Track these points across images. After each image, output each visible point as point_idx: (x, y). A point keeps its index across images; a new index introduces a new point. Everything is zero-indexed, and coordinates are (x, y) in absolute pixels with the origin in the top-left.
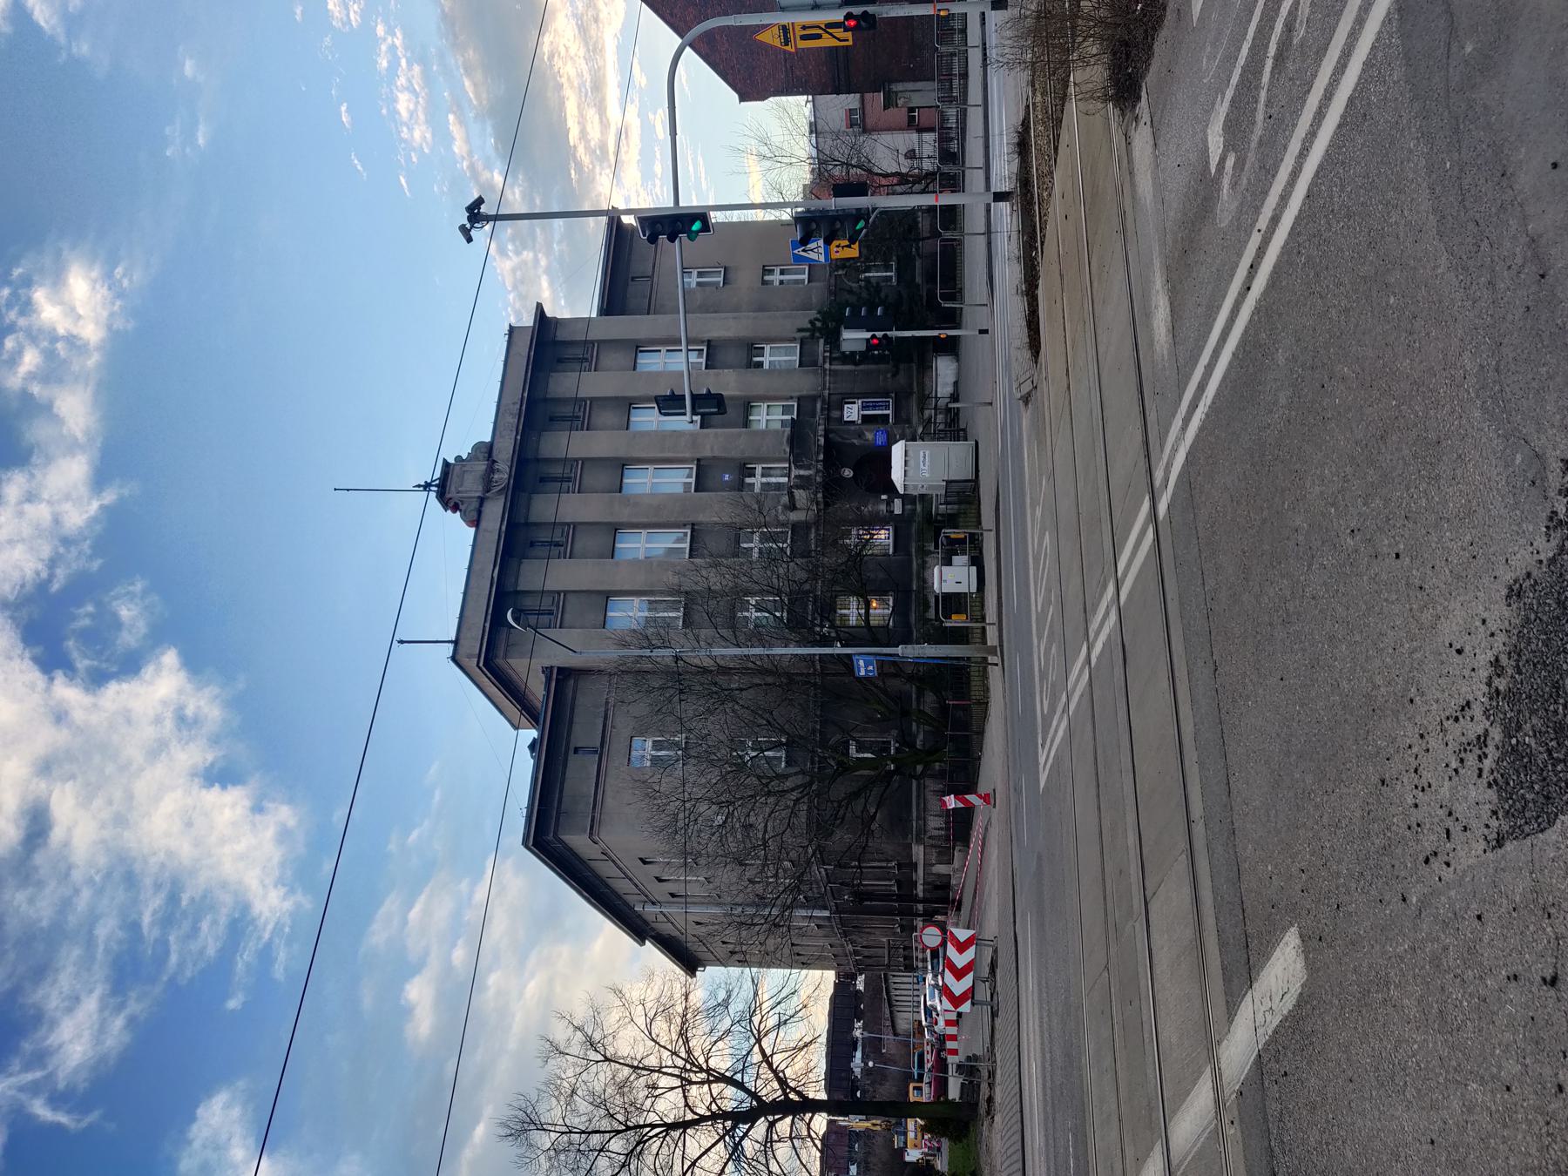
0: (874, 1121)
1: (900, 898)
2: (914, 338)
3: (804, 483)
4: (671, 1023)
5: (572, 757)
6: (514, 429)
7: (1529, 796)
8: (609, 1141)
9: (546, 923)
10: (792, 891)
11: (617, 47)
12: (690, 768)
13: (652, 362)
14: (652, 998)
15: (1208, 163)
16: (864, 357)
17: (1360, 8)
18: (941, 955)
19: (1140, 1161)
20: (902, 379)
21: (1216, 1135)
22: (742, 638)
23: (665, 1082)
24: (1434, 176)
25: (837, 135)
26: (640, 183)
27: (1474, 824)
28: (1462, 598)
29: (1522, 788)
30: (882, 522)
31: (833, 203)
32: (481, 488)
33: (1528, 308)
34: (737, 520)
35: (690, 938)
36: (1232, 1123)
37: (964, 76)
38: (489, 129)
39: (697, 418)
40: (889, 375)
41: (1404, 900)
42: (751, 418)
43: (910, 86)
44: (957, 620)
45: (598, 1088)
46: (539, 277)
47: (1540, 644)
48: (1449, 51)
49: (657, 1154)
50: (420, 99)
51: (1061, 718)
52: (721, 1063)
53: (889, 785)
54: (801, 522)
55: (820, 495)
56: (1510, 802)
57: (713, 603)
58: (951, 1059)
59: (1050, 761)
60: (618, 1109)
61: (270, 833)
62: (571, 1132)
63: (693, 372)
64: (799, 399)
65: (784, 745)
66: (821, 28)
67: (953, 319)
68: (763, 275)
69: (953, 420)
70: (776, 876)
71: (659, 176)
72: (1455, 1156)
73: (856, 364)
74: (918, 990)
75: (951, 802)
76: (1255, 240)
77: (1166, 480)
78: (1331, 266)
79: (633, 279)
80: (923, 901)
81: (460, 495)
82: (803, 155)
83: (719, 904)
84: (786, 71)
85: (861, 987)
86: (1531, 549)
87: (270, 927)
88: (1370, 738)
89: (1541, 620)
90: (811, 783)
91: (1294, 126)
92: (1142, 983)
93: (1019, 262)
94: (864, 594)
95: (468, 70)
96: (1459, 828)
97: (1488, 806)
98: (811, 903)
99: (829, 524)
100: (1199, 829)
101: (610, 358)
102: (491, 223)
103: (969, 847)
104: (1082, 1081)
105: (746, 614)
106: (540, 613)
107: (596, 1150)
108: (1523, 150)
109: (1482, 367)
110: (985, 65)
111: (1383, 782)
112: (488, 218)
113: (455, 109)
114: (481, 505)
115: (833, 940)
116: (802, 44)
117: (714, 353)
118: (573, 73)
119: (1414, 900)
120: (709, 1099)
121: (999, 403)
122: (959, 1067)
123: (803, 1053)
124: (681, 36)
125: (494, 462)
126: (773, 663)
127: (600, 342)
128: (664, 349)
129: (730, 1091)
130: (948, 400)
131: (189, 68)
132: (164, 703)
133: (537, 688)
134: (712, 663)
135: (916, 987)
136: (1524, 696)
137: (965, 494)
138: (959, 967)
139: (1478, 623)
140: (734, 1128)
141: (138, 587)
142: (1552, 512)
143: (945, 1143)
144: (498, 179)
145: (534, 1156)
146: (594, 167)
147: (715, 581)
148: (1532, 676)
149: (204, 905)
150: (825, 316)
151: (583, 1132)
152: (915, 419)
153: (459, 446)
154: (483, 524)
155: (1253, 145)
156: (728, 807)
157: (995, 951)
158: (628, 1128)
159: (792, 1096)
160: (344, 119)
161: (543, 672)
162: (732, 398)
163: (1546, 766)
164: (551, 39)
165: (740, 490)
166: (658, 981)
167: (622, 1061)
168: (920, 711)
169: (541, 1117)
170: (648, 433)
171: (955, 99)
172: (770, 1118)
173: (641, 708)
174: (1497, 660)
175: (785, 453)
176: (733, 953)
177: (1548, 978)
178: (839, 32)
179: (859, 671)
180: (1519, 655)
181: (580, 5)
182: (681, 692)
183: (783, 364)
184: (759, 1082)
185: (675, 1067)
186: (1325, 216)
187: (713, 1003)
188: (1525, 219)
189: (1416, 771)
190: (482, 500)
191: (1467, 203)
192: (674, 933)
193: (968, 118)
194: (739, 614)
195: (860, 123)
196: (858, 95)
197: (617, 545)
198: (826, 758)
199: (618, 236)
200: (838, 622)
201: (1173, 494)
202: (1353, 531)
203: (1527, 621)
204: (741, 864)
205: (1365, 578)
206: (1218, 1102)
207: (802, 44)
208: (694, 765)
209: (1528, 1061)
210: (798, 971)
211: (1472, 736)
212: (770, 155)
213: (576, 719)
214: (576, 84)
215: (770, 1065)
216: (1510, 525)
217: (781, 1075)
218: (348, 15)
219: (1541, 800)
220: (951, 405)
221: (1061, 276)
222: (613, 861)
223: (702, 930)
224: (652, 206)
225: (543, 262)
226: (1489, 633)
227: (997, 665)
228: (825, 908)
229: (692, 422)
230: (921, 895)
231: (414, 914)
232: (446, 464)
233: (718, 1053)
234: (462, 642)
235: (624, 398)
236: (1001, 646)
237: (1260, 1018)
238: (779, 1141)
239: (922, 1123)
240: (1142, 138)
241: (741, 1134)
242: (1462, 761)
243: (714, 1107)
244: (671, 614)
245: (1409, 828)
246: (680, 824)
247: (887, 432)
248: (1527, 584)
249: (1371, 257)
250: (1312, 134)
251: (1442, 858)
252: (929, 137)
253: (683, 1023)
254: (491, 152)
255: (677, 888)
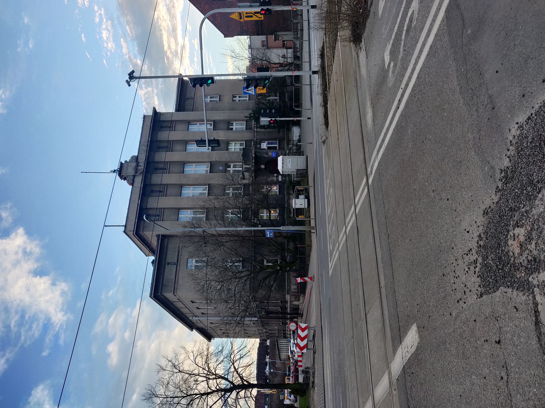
0: (273, 390)
1: (281, 313)
2: (285, 120)
3: (248, 170)
4: (202, 358)
5: (167, 266)
6: (146, 151)
7: (491, 281)
8: (181, 400)
9: (159, 323)
10: (244, 311)
11: (181, 16)
12: (208, 269)
13: (194, 128)
14: (196, 350)
15: (384, 65)
16: (268, 127)
17: (434, 16)
18: (296, 333)
19: (364, 403)
20: (281, 134)
21: (390, 393)
22: (226, 224)
23: (200, 379)
24: (458, 73)
25: (258, 49)
26: (189, 64)
27: (473, 289)
28: (469, 214)
29: (488, 278)
30: (275, 183)
31: (258, 74)
32: (134, 172)
33: (489, 119)
34: (225, 183)
35: (209, 328)
36: (395, 389)
37: (302, 30)
38: (136, 44)
39: (210, 148)
40: (277, 133)
41: (451, 315)
42: (229, 147)
43: (283, 33)
44: (301, 218)
45: (177, 382)
46: (154, 97)
47: (494, 230)
48: (463, 32)
49: (198, 404)
50: (111, 33)
51: (336, 252)
52: (220, 372)
53: (278, 274)
54: (247, 184)
55: (253, 174)
56: (485, 282)
57: (216, 212)
58: (300, 369)
59: (333, 266)
60: (184, 389)
61: (58, 293)
62: (167, 397)
63: (209, 132)
64: (246, 141)
65: (241, 261)
66: (252, 14)
67: (298, 114)
68: (233, 98)
69: (299, 149)
70: (239, 306)
71: (196, 62)
72: (468, 400)
73: (265, 129)
74: (288, 345)
75: (299, 280)
76: (400, 91)
77: (372, 171)
78: (425, 101)
79: (187, 99)
80: (289, 314)
81: (127, 174)
82: (247, 56)
83: (219, 316)
84: (240, 27)
85: (268, 344)
86: (490, 198)
87: (58, 326)
88: (439, 260)
89: (494, 222)
90: (251, 274)
91: (413, 54)
92: (365, 342)
93: (321, 95)
94: (269, 209)
95: (128, 23)
96: (468, 291)
97: (477, 284)
98: (251, 315)
99: (256, 184)
100: (383, 290)
101: (179, 127)
102: (137, 80)
103: (305, 295)
104: (345, 376)
105: (228, 216)
106: (156, 216)
107: (176, 403)
108: (487, 66)
109: (474, 137)
110: (309, 29)
111: (444, 275)
112: (136, 78)
113: (123, 37)
114: (134, 178)
115: (258, 328)
116: (246, 19)
117: (216, 125)
118: (165, 26)
119: (454, 315)
120: (216, 385)
121: (315, 143)
122: (303, 371)
123: (249, 368)
124: (204, 15)
125: (139, 163)
126: (237, 233)
127: (176, 121)
128: (198, 123)
129: (223, 381)
130: (297, 142)
131: (26, 20)
132: (19, 247)
133: (154, 242)
134: (216, 233)
135: (287, 343)
136: (489, 247)
137: (303, 174)
138: (302, 337)
139: (474, 223)
140: (225, 394)
141: (9, 205)
142: (497, 186)
143: (298, 397)
144: (139, 62)
145: (154, 406)
146: (173, 59)
147: (217, 204)
148: (491, 240)
149: (34, 318)
150: (255, 112)
151: (172, 397)
152: (286, 148)
153: (126, 157)
154: (135, 185)
155: (399, 60)
156: (222, 283)
157: (315, 331)
158: (188, 396)
159: (245, 383)
160: (83, 39)
161: (156, 236)
162: (223, 140)
163: (496, 271)
164: (158, 13)
165: (226, 173)
166: (198, 344)
167: (185, 372)
168: (288, 249)
169: (157, 392)
170: (193, 153)
171: (299, 38)
172: (237, 391)
173: (191, 249)
174: (480, 235)
175: (241, 159)
176: (224, 333)
177: (497, 341)
178: (259, 15)
179: (267, 235)
180: (487, 234)
181: (168, 1)
182: (205, 243)
183: (240, 128)
184: (234, 378)
185: (204, 373)
186: (423, 85)
187: (217, 351)
188: (487, 89)
189: (454, 272)
190: (134, 176)
191: (469, 83)
192: (204, 327)
193: (303, 45)
194: (225, 216)
195: (266, 46)
196: (265, 36)
197: (182, 192)
198: (256, 265)
199: (182, 84)
200: (260, 218)
201: (374, 176)
202: (433, 191)
203: (490, 222)
204: (227, 302)
205: (438, 207)
206: (390, 382)
207: (246, 19)
208: (210, 268)
209: (491, 369)
210: (246, 339)
211: (472, 260)
212: (235, 56)
213: (168, 253)
214: (166, 29)
215: (237, 372)
216: (484, 190)
217: (241, 375)
218: (84, 3)
219: (494, 282)
220: (298, 144)
221: (336, 100)
222: (182, 302)
223: (213, 326)
224: (194, 74)
225: (155, 92)
226: (477, 226)
227: (314, 233)
228: (256, 317)
229: (208, 149)
230: (289, 312)
231: (111, 321)
232: (122, 164)
233: (219, 368)
234: (127, 226)
235: (185, 140)
236: (316, 226)
237: (404, 355)
238: (241, 398)
239: (290, 391)
240: (362, 55)
241: (227, 396)
242: (469, 268)
243: (218, 387)
244: (201, 216)
245: (452, 291)
246: (205, 289)
247: (276, 152)
248: (489, 210)
249: (438, 99)
250: (419, 57)
251: (463, 301)
252: (290, 51)
253: (207, 358)
254: (136, 52)
255: (204, 311)
